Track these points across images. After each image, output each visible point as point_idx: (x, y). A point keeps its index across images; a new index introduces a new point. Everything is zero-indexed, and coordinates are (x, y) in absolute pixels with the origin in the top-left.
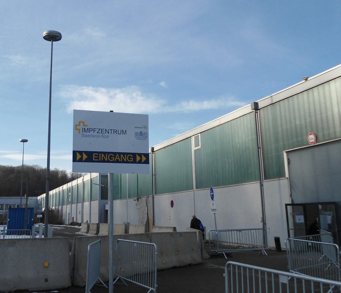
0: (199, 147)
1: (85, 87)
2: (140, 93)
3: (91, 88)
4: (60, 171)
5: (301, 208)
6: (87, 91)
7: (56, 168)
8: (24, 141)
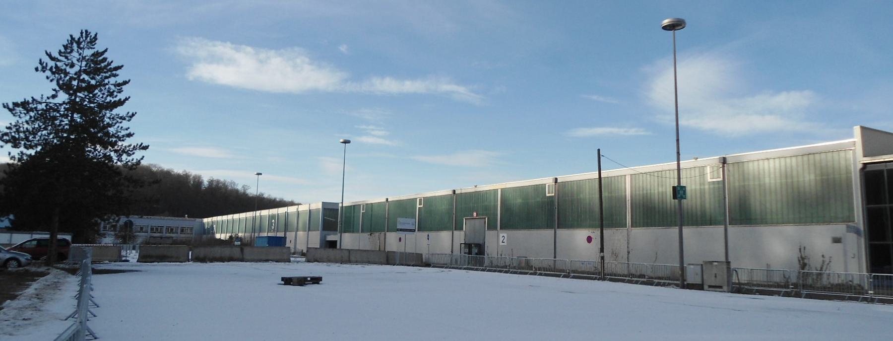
0: (422, 206)
1: (219, 43)
2: (307, 60)
3: (229, 44)
4: (215, 180)
5: (468, 246)
6: (224, 49)
7: (185, 171)
8: (258, 174)
